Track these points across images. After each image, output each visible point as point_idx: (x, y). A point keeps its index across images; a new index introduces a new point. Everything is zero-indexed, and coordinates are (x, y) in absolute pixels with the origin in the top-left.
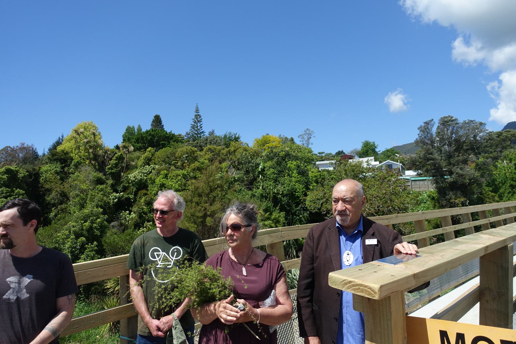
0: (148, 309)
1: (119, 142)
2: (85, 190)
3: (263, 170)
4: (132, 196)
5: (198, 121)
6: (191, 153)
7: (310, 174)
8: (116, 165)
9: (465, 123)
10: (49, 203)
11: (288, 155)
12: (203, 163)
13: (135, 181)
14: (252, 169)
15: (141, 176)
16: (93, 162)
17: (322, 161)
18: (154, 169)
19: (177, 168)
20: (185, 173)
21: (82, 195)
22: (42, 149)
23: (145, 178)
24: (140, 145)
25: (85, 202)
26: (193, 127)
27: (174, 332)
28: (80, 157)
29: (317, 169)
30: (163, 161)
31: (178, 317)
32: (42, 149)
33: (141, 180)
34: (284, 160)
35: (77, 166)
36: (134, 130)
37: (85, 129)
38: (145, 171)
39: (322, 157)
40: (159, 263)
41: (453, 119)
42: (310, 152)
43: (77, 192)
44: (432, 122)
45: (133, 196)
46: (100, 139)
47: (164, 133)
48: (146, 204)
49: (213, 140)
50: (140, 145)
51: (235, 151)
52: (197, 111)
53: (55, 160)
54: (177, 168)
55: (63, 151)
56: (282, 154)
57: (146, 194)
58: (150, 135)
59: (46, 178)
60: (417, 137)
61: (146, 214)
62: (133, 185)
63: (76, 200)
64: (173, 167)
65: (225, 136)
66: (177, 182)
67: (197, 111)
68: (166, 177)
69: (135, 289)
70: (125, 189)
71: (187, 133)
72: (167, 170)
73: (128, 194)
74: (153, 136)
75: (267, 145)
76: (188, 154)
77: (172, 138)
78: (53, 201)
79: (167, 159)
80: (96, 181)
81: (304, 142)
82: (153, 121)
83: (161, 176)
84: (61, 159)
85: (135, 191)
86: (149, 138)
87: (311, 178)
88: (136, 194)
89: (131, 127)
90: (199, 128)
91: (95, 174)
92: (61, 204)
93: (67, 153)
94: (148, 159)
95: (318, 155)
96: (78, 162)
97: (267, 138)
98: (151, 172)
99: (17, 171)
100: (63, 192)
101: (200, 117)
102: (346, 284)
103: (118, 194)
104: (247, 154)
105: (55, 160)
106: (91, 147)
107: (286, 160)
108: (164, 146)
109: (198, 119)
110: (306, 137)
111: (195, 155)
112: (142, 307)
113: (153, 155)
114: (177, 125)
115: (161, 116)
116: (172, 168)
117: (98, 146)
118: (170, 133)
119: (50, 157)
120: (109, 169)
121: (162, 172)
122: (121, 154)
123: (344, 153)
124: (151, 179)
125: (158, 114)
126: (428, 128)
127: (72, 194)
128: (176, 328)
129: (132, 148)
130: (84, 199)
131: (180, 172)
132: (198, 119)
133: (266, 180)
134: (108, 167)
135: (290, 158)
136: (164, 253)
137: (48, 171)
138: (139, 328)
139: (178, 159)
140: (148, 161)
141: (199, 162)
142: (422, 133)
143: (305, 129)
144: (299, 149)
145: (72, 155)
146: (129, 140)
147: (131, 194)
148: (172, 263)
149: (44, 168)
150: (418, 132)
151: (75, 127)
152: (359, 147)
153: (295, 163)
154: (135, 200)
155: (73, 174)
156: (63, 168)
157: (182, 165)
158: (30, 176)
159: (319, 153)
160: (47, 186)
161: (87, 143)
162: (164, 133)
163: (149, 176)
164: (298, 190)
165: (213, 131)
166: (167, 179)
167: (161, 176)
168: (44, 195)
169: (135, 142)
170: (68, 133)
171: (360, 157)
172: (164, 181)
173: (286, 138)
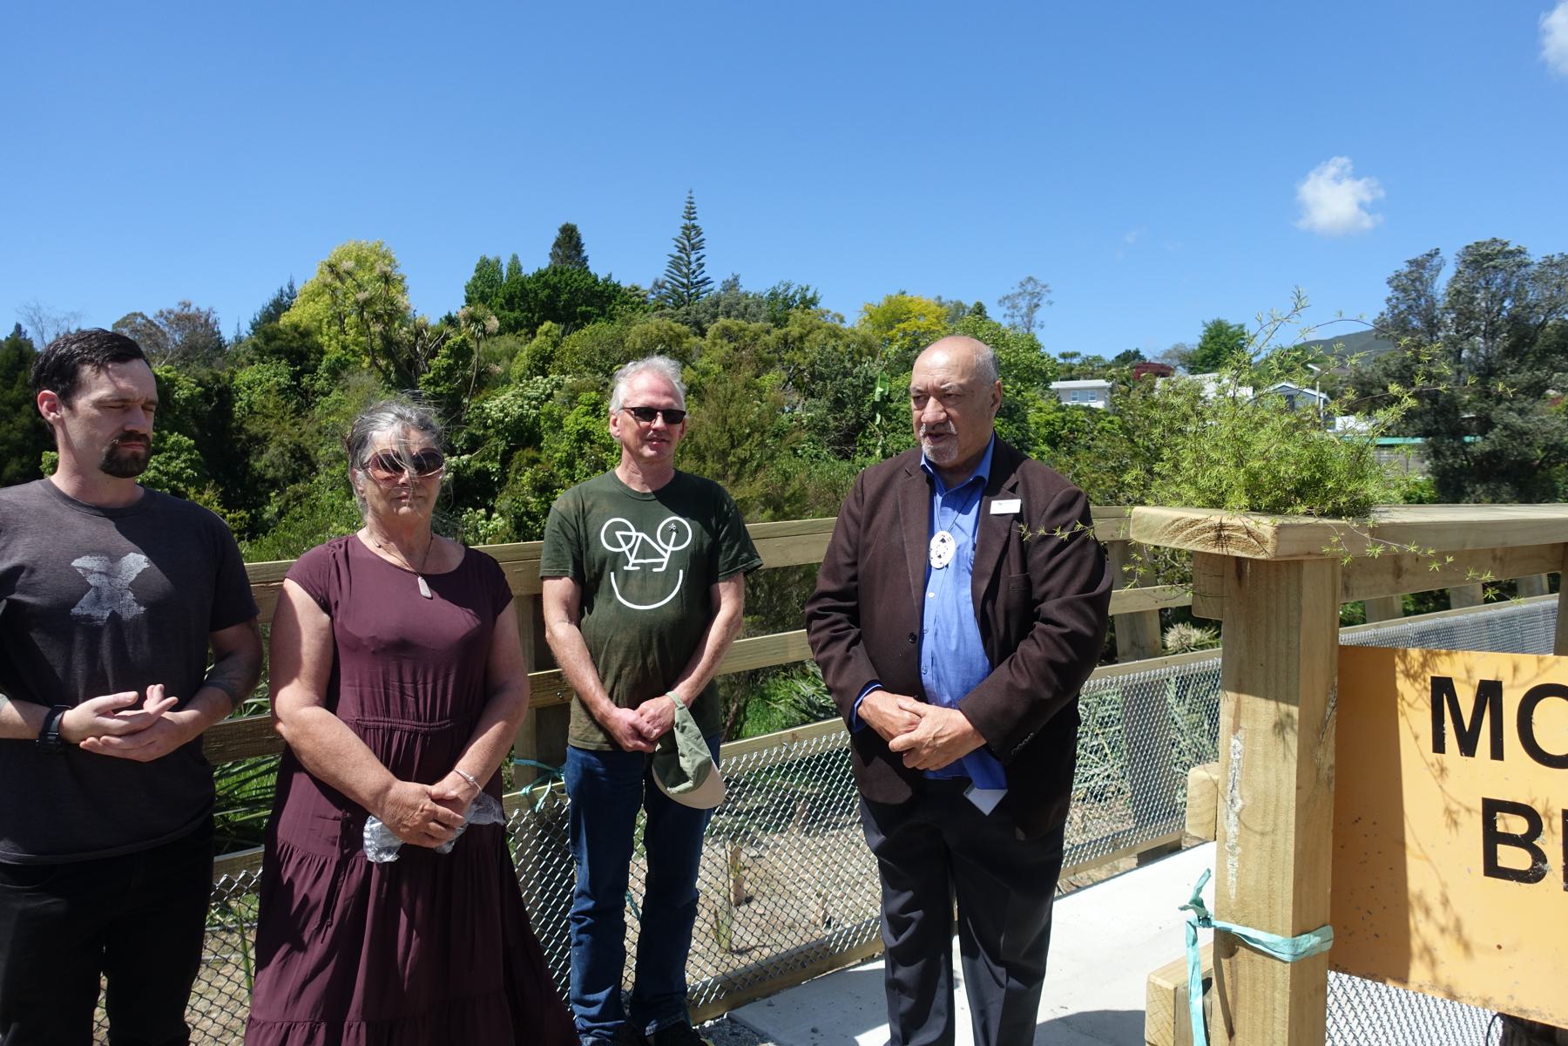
1: (456, 305)
3: (886, 399)
4: (493, 467)
7: (1033, 417)
8: (450, 370)
9: (1550, 263)
12: (705, 373)
13: (502, 422)
14: (855, 393)
15: (521, 407)
16: (383, 363)
17: (1071, 379)
18: (559, 386)
22: (235, 322)
23: (534, 412)
24: (517, 314)
26: (676, 263)
27: (679, 737)
30: (587, 364)
32: (235, 322)
35: (336, 371)
36: (500, 273)
37: (360, 262)
38: (534, 394)
40: (632, 560)
41: (1512, 247)
42: (1034, 347)
44: (1436, 261)
47: (590, 281)
48: (535, 489)
49: (734, 304)
51: (801, 338)
52: (690, 213)
53: (273, 352)
55: (295, 327)
58: (546, 285)
59: (250, 405)
60: (1384, 308)
61: (535, 519)
62: (498, 433)
63: (334, 472)
65: (774, 295)
67: (690, 213)
68: (594, 410)
70: (474, 444)
71: (656, 284)
72: (597, 390)
73: (483, 460)
74: (555, 288)
75: (902, 326)
78: (270, 473)
81: (1018, 319)
82: (557, 245)
83: (581, 409)
85: (505, 453)
86: (543, 295)
87: (1033, 427)
90: (694, 266)
92: (294, 480)
93: (306, 334)
94: (542, 358)
95: (1061, 361)
96: (338, 360)
97: (903, 303)
98: (550, 396)
99: (172, 382)
102: (1181, 529)
103: (454, 459)
104: (841, 348)
109: (691, 239)
110: (1023, 304)
111: (685, 346)
112: (587, 679)
113: (555, 344)
114: (628, 259)
115: (580, 230)
117: (393, 314)
118: (605, 281)
119: (260, 342)
120: (428, 382)
121: (583, 397)
122: (464, 341)
123: (1141, 358)
125: (572, 222)
126: (1419, 279)
129: (493, 323)
132: (691, 239)
133: (894, 430)
134: (426, 376)
136: (641, 535)
137: (257, 382)
140: (542, 363)
141: (694, 368)
142: (1401, 296)
143: (1023, 278)
145: (322, 340)
146: (484, 298)
147: (493, 460)
148: (666, 561)
149: (245, 376)
150: (1388, 292)
152: (1192, 339)
154: (504, 479)
156: (296, 376)
158: (207, 396)
159: (1064, 356)
160: (254, 428)
163: (545, 408)
165: (736, 279)
166: (598, 416)
167: (581, 409)
168: (246, 453)
169: (502, 307)
170: (308, 275)
171: (1193, 371)
172: (588, 422)
173: (959, 306)
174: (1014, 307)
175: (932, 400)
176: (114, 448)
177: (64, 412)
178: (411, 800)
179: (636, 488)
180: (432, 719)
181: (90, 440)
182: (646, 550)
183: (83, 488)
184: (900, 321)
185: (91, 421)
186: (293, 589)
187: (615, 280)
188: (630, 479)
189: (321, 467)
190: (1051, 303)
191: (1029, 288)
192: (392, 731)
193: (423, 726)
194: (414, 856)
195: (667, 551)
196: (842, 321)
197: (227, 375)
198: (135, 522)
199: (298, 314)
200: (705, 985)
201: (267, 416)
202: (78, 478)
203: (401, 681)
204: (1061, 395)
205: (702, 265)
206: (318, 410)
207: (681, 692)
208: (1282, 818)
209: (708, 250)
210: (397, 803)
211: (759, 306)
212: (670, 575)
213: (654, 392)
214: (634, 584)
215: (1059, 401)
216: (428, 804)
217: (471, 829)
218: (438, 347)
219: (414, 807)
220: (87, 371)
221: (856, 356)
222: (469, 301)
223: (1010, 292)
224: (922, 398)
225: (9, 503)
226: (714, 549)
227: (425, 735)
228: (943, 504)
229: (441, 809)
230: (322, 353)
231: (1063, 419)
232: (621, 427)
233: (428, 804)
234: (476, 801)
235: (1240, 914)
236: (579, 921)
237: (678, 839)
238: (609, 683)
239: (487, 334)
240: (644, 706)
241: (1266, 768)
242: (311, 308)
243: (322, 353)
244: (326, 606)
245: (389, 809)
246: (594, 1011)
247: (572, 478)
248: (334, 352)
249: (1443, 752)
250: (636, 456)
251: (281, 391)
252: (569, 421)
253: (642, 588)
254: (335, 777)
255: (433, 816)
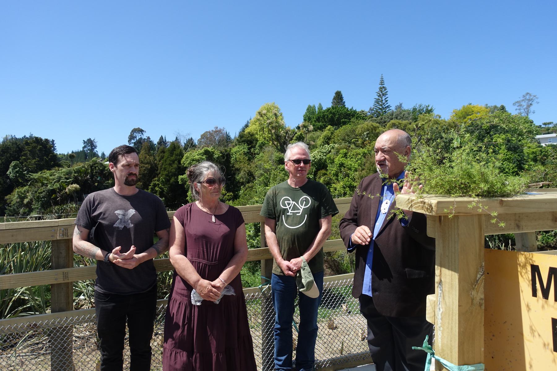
0: (281, 252)
2: (268, 170)
5: (383, 95)
6: (372, 129)
7: (526, 150)
10: (239, 182)
11: (494, 128)
13: (314, 161)
16: (276, 143)
17: (549, 133)
18: (333, 148)
19: (357, 146)
20: (366, 151)
21: (265, 174)
22: (234, 134)
24: (321, 124)
25: (269, 181)
26: (377, 101)
27: (302, 272)
28: (265, 139)
29: (536, 143)
30: (343, 140)
31: (307, 260)
32: (234, 134)
33: (320, 159)
34: (488, 133)
35: (262, 146)
36: (315, 109)
37: (268, 111)
38: (324, 151)
39: (548, 129)
40: (290, 211)
43: (262, 172)
45: (313, 176)
46: (282, 119)
47: (345, 110)
50: (321, 124)
52: (382, 83)
53: (243, 142)
54: (357, 146)
55: (249, 133)
56: (486, 126)
57: (325, 174)
59: (236, 159)
63: (260, 180)
64: (353, 146)
65: (415, 109)
66: (357, 161)
67: (382, 83)
68: (345, 156)
69: (268, 232)
71: (370, 109)
72: (346, 149)
74: (334, 114)
75: (469, 117)
76: (369, 130)
77: (353, 116)
78: (241, 180)
79: (347, 137)
80: (279, 161)
81: (522, 111)
82: (334, 99)
83: (340, 155)
84: (248, 141)
86: (330, 116)
87: (526, 154)
88: (315, 174)
89: (312, 106)
90: (384, 102)
91: (278, 154)
92: (248, 182)
93: (252, 135)
94: (328, 138)
95: (544, 126)
96: (262, 143)
97: (469, 108)
99: (213, 152)
100: (249, 171)
101: (385, 90)
104: (439, 128)
105: (243, 142)
106: (273, 128)
107: (491, 133)
108: (345, 123)
110: (524, 104)
111: (377, 131)
112: (275, 250)
113: (332, 133)
114: (360, 101)
115: (342, 93)
116: (351, 146)
117: (278, 127)
118: (351, 110)
119: (239, 139)
121: (341, 151)
122: (301, 134)
124: (330, 158)
125: (339, 90)
127: (257, 174)
128: (304, 269)
129: (311, 128)
130: (267, 178)
131: (361, 151)
135: (497, 131)
136: (294, 202)
137: (238, 151)
138: (273, 268)
139: (358, 137)
140: (327, 140)
143: (524, 94)
144: (510, 119)
145: (257, 136)
146: (309, 119)
148: (301, 211)
149: (234, 150)
151: (259, 110)
153: (504, 136)
155: (258, 154)
156: (249, 149)
157: (363, 143)
158: (223, 156)
159: (545, 124)
160: (237, 166)
161: (270, 124)
162: (345, 110)
163: (328, 156)
164: (507, 170)
165: (401, 105)
166: (346, 158)
167: (340, 155)
168: (234, 174)
169: (315, 122)
170: (254, 116)
172: (343, 160)
173: (495, 107)
174: (520, 105)
175: (380, 152)
176: (127, 178)
177: (115, 168)
178: (205, 285)
179: (293, 186)
180: (212, 261)
181: (121, 176)
182: (295, 208)
183: (121, 190)
184: (468, 115)
185: (121, 171)
186: (175, 219)
187: (354, 109)
188: (291, 183)
189: (256, 178)
190: (538, 103)
191: (528, 97)
192: (200, 263)
193: (209, 263)
194: (206, 304)
195: (302, 208)
196: (440, 117)
197: (229, 149)
198: (133, 200)
199: (252, 128)
200: (325, 361)
201: (241, 162)
202: (119, 187)
203: (203, 248)
204: (541, 141)
205: (387, 101)
206: (256, 159)
207: (306, 256)
208: (454, 317)
209: (389, 95)
210: (201, 285)
211: (409, 114)
212: (302, 217)
213: (299, 154)
214: (290, 220)
215: (539, 143)
216: (210, 287)
217: (225, 297)
218: (293, 137)
219: (205, 287)
220: (120, 157)
221: (447, 130)
222: (305, 120)
223: (519, 100)
224: (377, 151)
225: (102, 195)
226: (319, 208)
227: (209, 266)
228: (387, 190)
229: (214, 289)
230: (257, 141)
231: (541, 151)
232: (289, 166)
233: (210, 287)
234: (226, 288)
235: (442, 354)
236: (276, 332)
237: (309, 308)
238: (282, 252)
239: (309, 131)
240: (292, 260)
241: (449, 297)
242: (254, 127)
243: (257, 141)
244: (183, 224)
245: (198, 287)
246: (280, 363)
247: (337, 180)
248: (261, 140)
249: (536, 296)
250: (295, 176)
251: (245, 154)
252: (336, 160)
253: (292, 221)
254: (184, 277)
255: (211, 291)
